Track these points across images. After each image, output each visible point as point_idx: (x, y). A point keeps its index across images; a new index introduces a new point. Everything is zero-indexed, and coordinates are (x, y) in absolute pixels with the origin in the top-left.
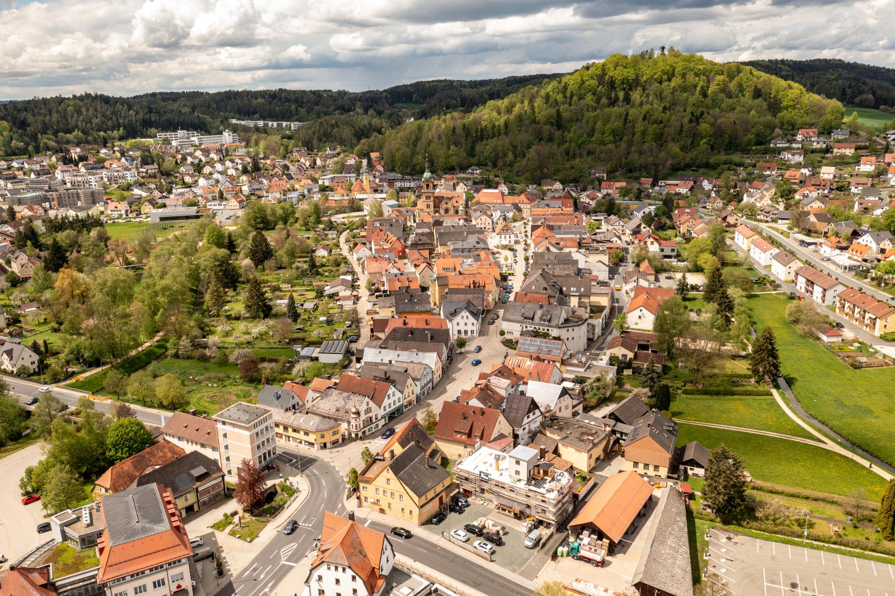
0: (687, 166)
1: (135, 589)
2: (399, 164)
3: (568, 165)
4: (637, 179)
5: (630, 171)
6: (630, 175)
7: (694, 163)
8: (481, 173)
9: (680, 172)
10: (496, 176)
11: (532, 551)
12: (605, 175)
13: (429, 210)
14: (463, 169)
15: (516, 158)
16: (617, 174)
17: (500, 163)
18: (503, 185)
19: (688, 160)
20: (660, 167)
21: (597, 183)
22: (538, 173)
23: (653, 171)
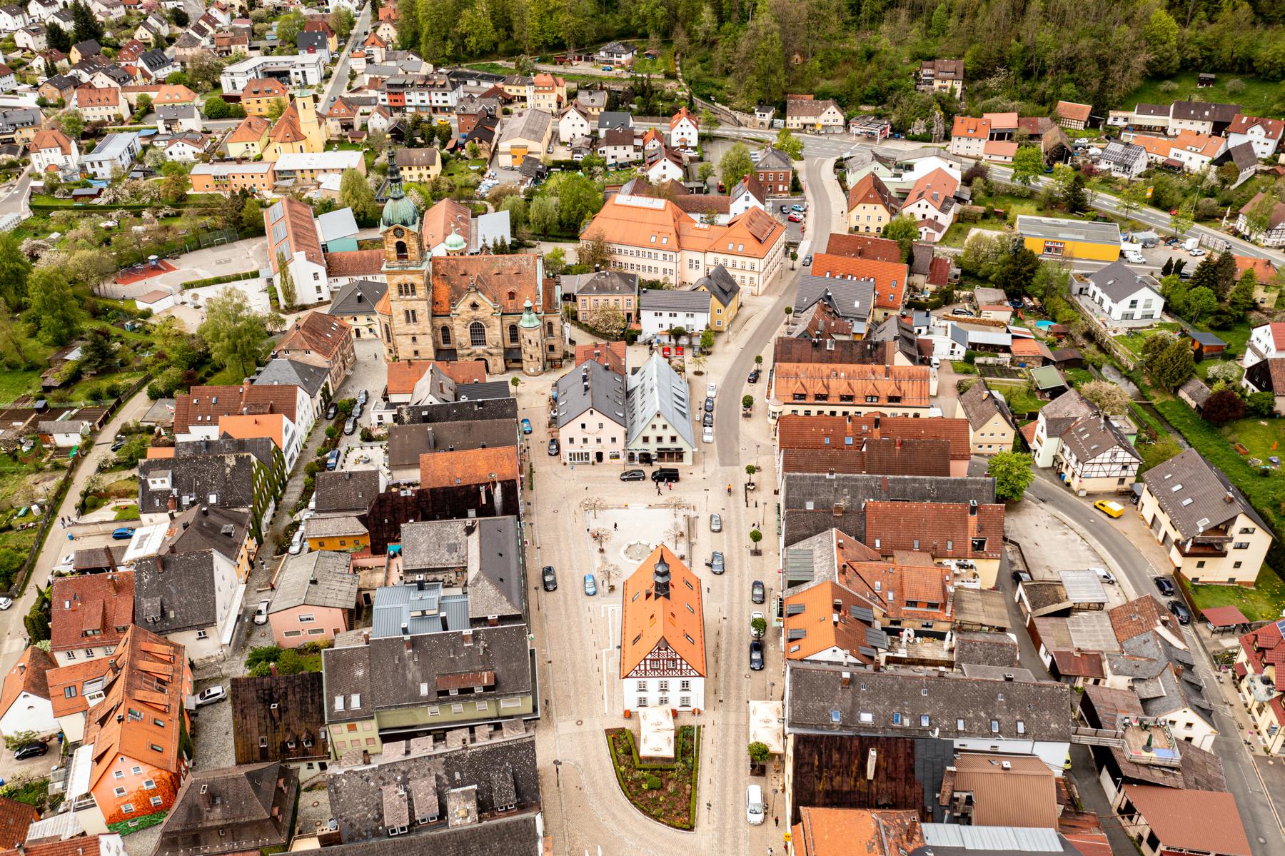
0: (1188, 68)
1: (400, 286)
2: (426, 29)
3: (854, 43)
4: (1046, 103)
5: (1027, 75)
6: (1027, 86)
7: (1209, 59)
8: (632, 67)
9: (1169, 85)
10: (670, 76)
11: (755, 829)
12: (958, 86)
13: (413, 328)
14: (586, 46)
15: (721, 21)
16: (992, 83)
17: (680, 39)
18: (685, 121)
19: (1193, 52)
20: (1116, 69)
21: (939, 114)
22: (780, 78)
23: (1096, 84)
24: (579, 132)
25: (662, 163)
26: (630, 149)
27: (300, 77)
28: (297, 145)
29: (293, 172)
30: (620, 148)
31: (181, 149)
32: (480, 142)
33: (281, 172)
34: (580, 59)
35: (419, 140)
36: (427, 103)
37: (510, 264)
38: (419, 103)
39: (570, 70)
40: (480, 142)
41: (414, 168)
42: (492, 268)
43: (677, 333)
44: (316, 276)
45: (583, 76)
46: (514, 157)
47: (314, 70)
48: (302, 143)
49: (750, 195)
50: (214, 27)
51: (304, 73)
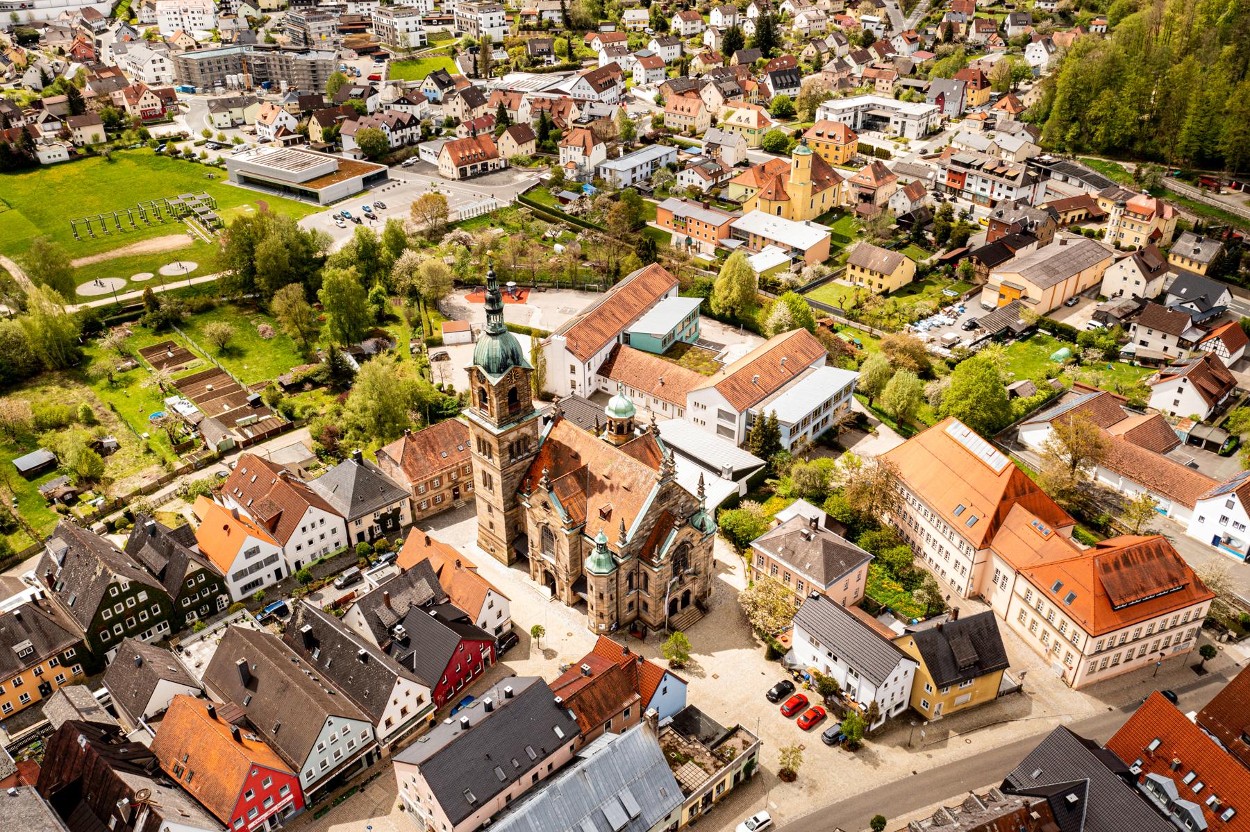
24: (1130, 290)
25: (1178, 382)
26: (1172, 341)
27: (898, 128)
28: (775, 205)
29: (747, 234)
30: (1157, 335)
31: (691, 176)
32: (978, 263)
33: (736, 230)
34: (1238, 187)
35: (930, 236)
36: (988, 193)
37: (626, 470)
38: (978, 191)
39: (1212, 199)
40: (978, 263)
41: (867, 273)
42: (605, 465)
43: (829, 689)
44: (573, 369)
45: (1222, 212)
46: (1002, 296)
47: (916, 123)
48: (783, 205)
49: (1236, 500)
50: (882, 55)
51: (904, 123)
